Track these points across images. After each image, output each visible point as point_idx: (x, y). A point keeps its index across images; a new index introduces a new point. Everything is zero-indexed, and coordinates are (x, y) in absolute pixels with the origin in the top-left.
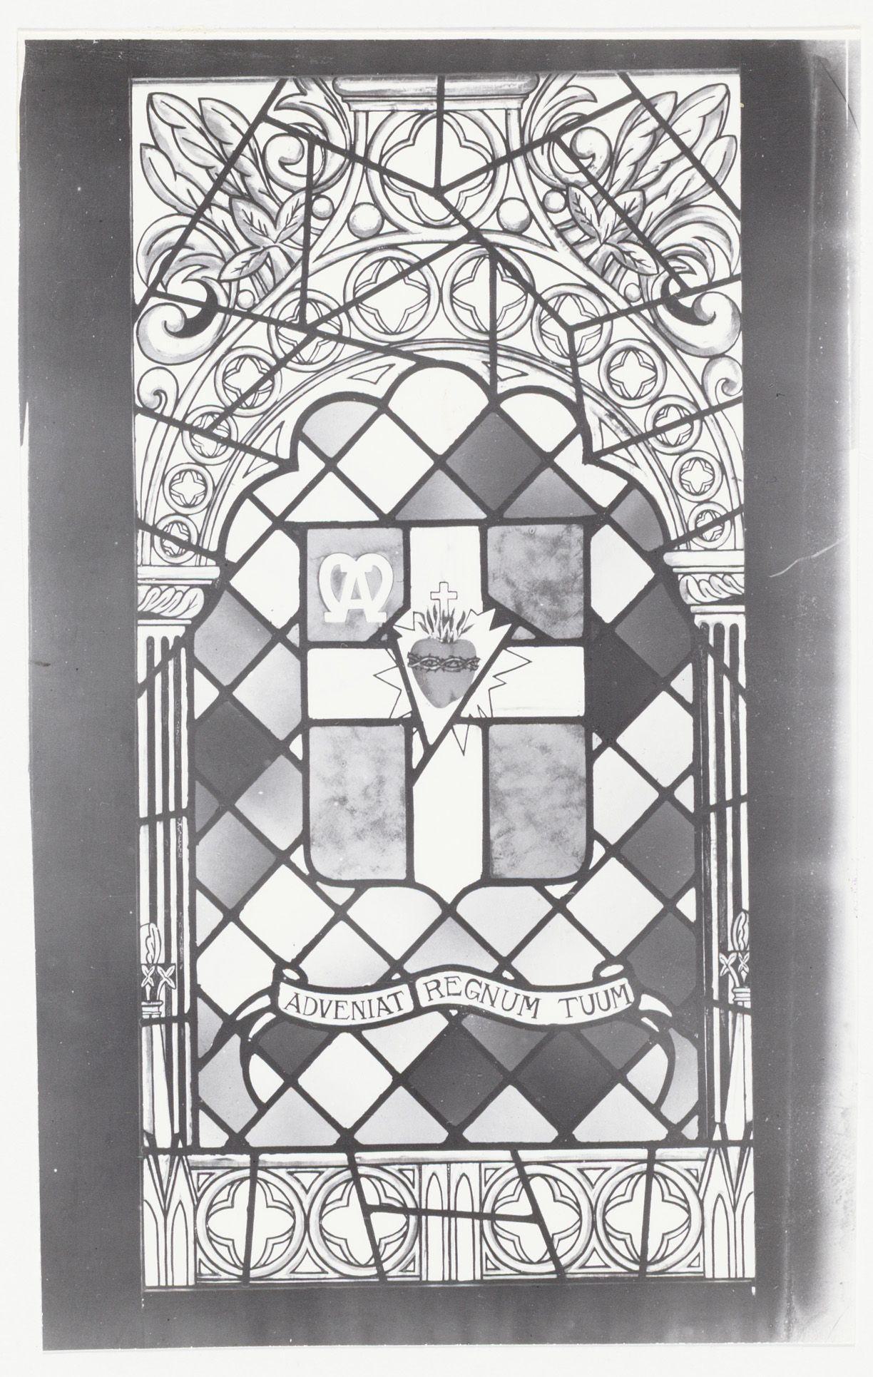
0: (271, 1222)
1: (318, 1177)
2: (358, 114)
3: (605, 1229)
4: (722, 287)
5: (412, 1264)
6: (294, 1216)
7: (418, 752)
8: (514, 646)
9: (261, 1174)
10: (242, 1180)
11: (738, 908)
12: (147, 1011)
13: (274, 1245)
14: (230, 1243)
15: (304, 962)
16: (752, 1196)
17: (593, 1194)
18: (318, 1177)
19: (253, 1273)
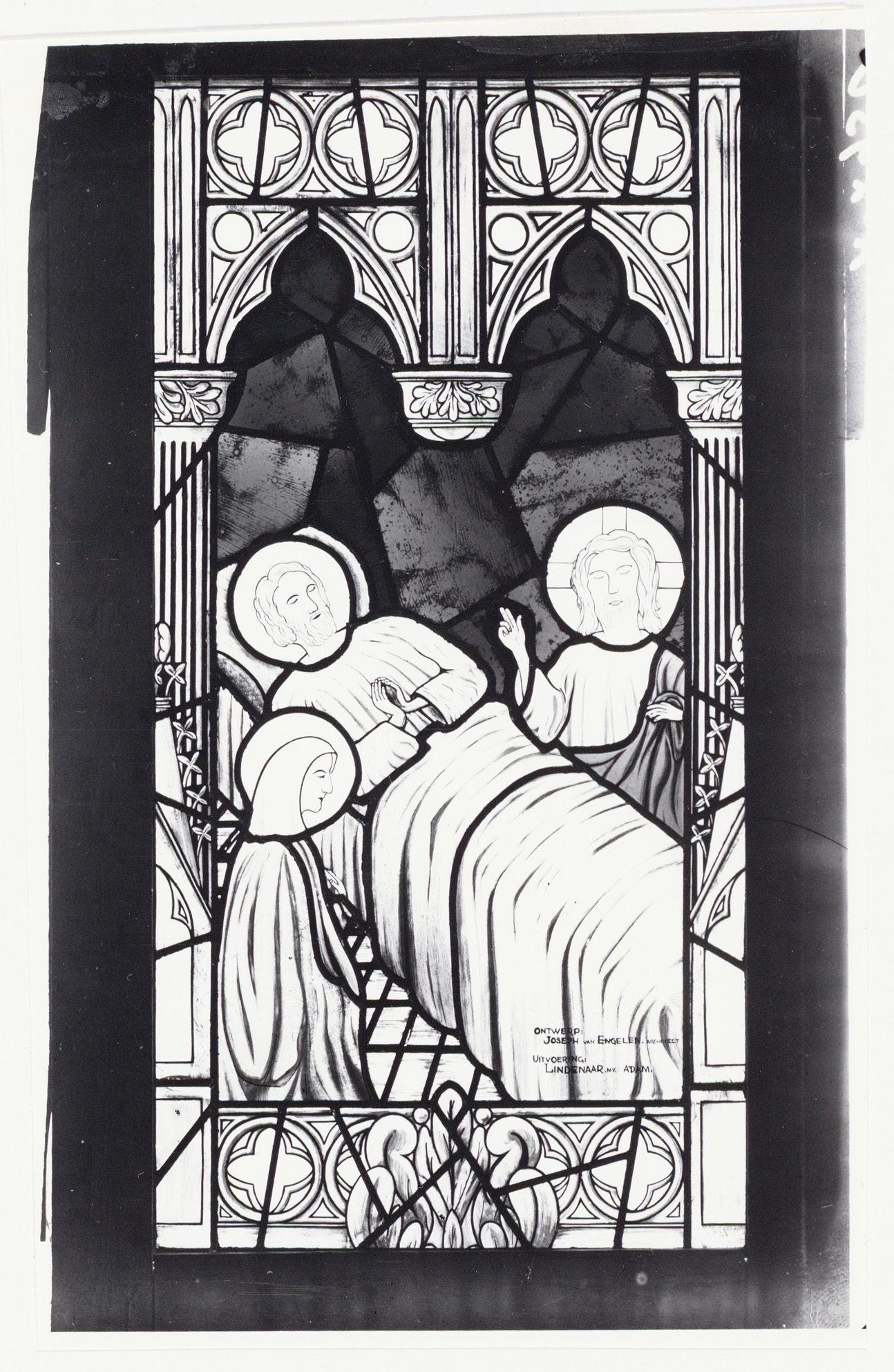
0: (280, 141)
1: (313, 1214)
2: (400, 725)
3: (602, 152)
4: (744, 892)
5: (410, 96)
6: (300, 137)
7: (426, 1233)
8: (528, 1154)
9: (257, 1217)
10: (252, 101)
11: (738, 622)
12: (161, 705)
13: (280, 120)
14: (238, 161)
15: (315, 835)
16: (742, 878)
17: (581, 1147)
18: (313, 1214)
19: (260, 93)
